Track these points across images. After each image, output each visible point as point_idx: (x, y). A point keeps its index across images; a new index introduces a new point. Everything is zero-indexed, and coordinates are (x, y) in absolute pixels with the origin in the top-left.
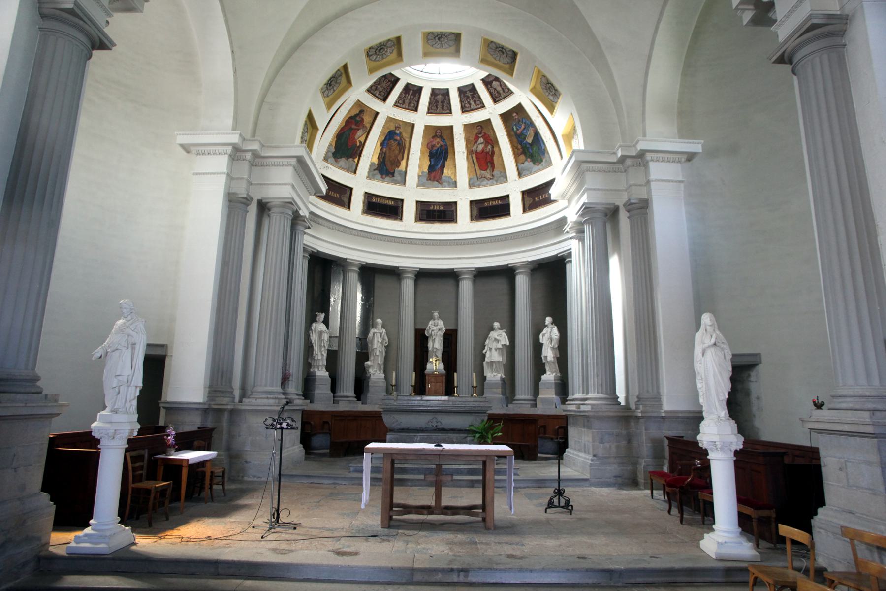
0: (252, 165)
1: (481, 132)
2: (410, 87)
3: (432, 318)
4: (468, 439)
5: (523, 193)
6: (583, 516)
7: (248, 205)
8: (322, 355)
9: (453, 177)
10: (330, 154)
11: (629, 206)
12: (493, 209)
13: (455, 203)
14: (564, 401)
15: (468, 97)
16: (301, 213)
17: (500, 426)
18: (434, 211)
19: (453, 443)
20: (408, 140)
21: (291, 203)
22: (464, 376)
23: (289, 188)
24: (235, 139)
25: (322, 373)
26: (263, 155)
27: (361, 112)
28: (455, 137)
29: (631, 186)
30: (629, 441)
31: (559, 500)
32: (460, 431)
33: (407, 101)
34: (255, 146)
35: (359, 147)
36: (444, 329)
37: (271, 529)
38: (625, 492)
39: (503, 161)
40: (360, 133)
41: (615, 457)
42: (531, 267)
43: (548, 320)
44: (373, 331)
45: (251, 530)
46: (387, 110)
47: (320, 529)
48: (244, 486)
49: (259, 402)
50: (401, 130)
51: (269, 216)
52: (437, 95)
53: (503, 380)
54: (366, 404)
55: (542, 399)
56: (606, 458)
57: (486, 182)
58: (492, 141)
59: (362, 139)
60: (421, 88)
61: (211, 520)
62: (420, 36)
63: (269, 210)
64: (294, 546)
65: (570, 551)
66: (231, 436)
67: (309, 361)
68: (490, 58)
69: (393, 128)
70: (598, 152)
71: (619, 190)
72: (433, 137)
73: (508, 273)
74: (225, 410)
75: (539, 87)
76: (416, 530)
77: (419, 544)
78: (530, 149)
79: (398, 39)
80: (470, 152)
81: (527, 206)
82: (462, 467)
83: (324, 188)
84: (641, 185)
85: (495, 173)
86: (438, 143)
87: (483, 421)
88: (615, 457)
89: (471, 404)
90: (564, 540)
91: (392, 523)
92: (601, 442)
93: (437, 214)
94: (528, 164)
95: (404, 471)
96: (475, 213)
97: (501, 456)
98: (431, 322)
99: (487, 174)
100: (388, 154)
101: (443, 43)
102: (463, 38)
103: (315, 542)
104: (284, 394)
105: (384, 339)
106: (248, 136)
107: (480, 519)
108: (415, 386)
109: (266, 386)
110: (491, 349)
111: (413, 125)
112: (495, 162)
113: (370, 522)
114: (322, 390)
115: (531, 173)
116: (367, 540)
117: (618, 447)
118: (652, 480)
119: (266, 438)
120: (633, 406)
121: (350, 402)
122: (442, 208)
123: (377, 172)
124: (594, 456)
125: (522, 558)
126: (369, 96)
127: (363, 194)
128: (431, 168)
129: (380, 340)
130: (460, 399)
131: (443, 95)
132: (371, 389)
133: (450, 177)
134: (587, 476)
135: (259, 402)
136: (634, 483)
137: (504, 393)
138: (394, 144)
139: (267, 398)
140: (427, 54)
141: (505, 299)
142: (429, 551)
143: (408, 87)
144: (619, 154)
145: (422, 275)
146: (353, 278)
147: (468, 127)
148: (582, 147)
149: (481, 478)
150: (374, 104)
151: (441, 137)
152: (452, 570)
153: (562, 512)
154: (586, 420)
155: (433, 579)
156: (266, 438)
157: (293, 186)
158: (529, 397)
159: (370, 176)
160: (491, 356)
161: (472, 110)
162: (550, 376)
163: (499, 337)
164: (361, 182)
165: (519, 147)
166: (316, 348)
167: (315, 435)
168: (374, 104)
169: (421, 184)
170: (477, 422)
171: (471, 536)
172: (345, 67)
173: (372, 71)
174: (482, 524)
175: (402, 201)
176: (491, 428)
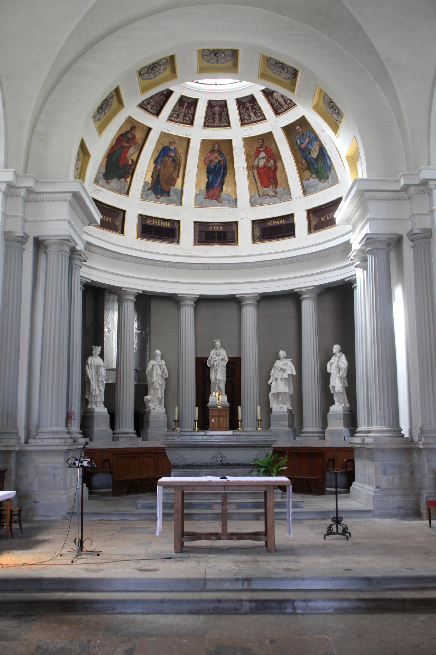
0: (26, 200)
1: (263, 145)
2: (185, 100)
3: (214, 347)
4: (254, 473)
5: (309, 211)
6: (359, 541)
7: (24, 243)
8: (100, 390)
9: (232, 195)
10: (101, 176)
11: (412, 235)
12: (275, 229)
13: (236, 223)
14: (353, 433)
15: (247, 109)
16: (78, 248)
17: (284, 460)
18: (213, 232)
19: (237, 476)
20: (183, 156)
21: (69, 240)
22: (250, 409)
23: (66, 224)
24: (9, 176)
25: (100, 409)
26: (37, 191)
27: (133, 128)
28: (235, 152)
29: (414, 215)
30: (412, 473)
31: (337, 526)
32: (245, 466)
33: (182, 115)
34: (30, 183)
35: (131, 166)
36: (227, 359)
37: (77, 556)
38: (406, 522)
39: (286, 178)
40: (132, 150)
41: (398, 489)
42: (317, 291)
43: (336, 348)
44: (152, 363)
45: (59, 557)
46: (160, 125)
47: (120, 555)
48: (36, 525)
49: (46, 442)
50: (176, 146)
51: (46, 253)
52: (215, 106)
53: (290, 411)
54: (146, 440)
55: (330, 431)
56: (390, 489)
57: (269, 199)
58: (274, 155)
59: (134, 157)
60: (196, 101)
61: (19, 552)
62: (195, 53)
63: (46, 247)
64: (101, 567)
65: (339, 565)
66: (18, 477)
67: (87, 397)
68: (270, 73)
69: (167, 144)
70: (381, 181)
71: (403, 219)
72: (211, 152)
73: (294, 297)
74: (13, 451)
75: (321, 104)
76: (205, 553)
77: (209, 563)
78: (316, 165)
79: (172, 58)
80: (250, 167)
81: (312, 226)
82: (247, 501)
83: (98, 217)
84: (424, 214)
85: (279, 189)
86: (216, 158)
87: (267, 455)
88: (398, 489)
89: (256, 439)
90: (334, 559)
91: (184, 549)
92: (385, 474)
93: (216, 235)
94: (314, 180)
95: (191, 506)
96: (258, 233)
97: (283, 488)
98: (213, 352)
99: (270, 190)
100: (162, 172)
101: (221, 60)
102: (240, 54)
103: (119, 564)
104: (69, 433)
105: (163, 371)
106: (21, 173)
107: (263, 543)
108: (198, 421)
109: (51, 426)
110: (276, 379)
111: (189, 139)
112: (278, 179)
113: (163, 549)
114: (101, 427)
115: (316, 191)
116: (164, 562)
117: (401, 479)
118: (429, 510)
119: (54, 477)
120: (416, 439)
121: (131, 438)
122: (221, 228)
123: (150, 191)
124: (377, 487)
125: (296, 570)
126: (141, 112)
127: (136, 216)
128: (209, 186)
129: (159, 372)
130: (245, 433)
131: (220, 106)
132: (151, 424)
133: (229, 195)
134: (371, 508)
135: (46, 442)
136: (417, 514)
137: (291, 425)
138: (168, 161)
139: (53, 438)
140: (203, 70)
141: (293, 322)
142: (218, 567)
143: (182, 100)
144: (402, 183)
145: (202, 301)
146: (130, 307)
147: (248, 141)
148: (365, 177)
149: (263, 511)
150: (145, 119)
151: (219, 152)
152: (237, 579)
153: (340, 539)
154: (370, 452)
155: (222, 588)
156: (54, 477)
157: (69, 223)
158: (318, 429)
159: (144, 197)
160: (277, 387)
161: (252, 122)
162: (338, 407)
163: (284, 367)
164: (135, 204)
165: (304, 162)
166: (93, 383)
167: (95, 474)
168: (145, 119)
169: (198, 204)
170: (262, 456)
171: (254, 557)
172: (117, 90)
173: (144, 90)
174: (265, 549)
175: (179, 222)
176: (276, 461)
